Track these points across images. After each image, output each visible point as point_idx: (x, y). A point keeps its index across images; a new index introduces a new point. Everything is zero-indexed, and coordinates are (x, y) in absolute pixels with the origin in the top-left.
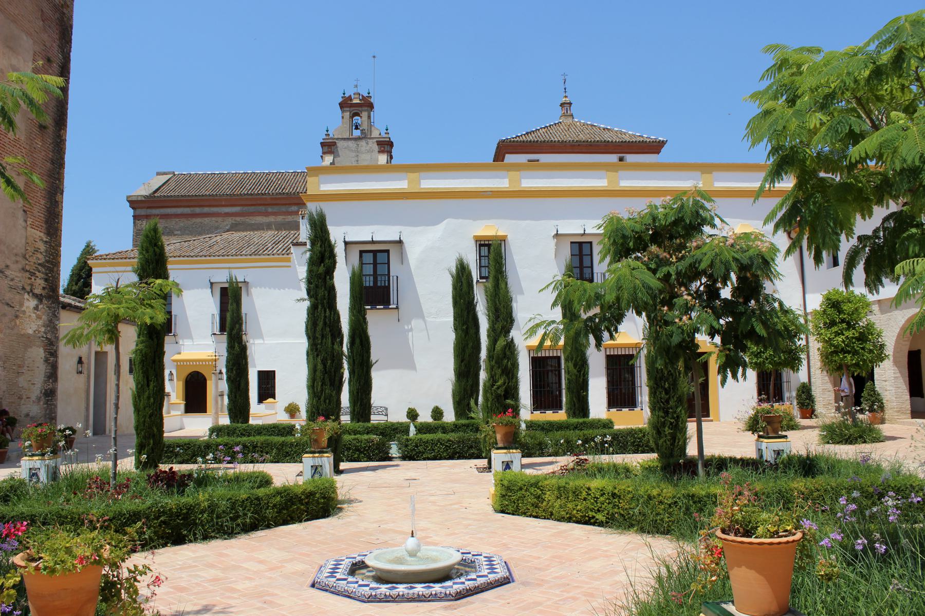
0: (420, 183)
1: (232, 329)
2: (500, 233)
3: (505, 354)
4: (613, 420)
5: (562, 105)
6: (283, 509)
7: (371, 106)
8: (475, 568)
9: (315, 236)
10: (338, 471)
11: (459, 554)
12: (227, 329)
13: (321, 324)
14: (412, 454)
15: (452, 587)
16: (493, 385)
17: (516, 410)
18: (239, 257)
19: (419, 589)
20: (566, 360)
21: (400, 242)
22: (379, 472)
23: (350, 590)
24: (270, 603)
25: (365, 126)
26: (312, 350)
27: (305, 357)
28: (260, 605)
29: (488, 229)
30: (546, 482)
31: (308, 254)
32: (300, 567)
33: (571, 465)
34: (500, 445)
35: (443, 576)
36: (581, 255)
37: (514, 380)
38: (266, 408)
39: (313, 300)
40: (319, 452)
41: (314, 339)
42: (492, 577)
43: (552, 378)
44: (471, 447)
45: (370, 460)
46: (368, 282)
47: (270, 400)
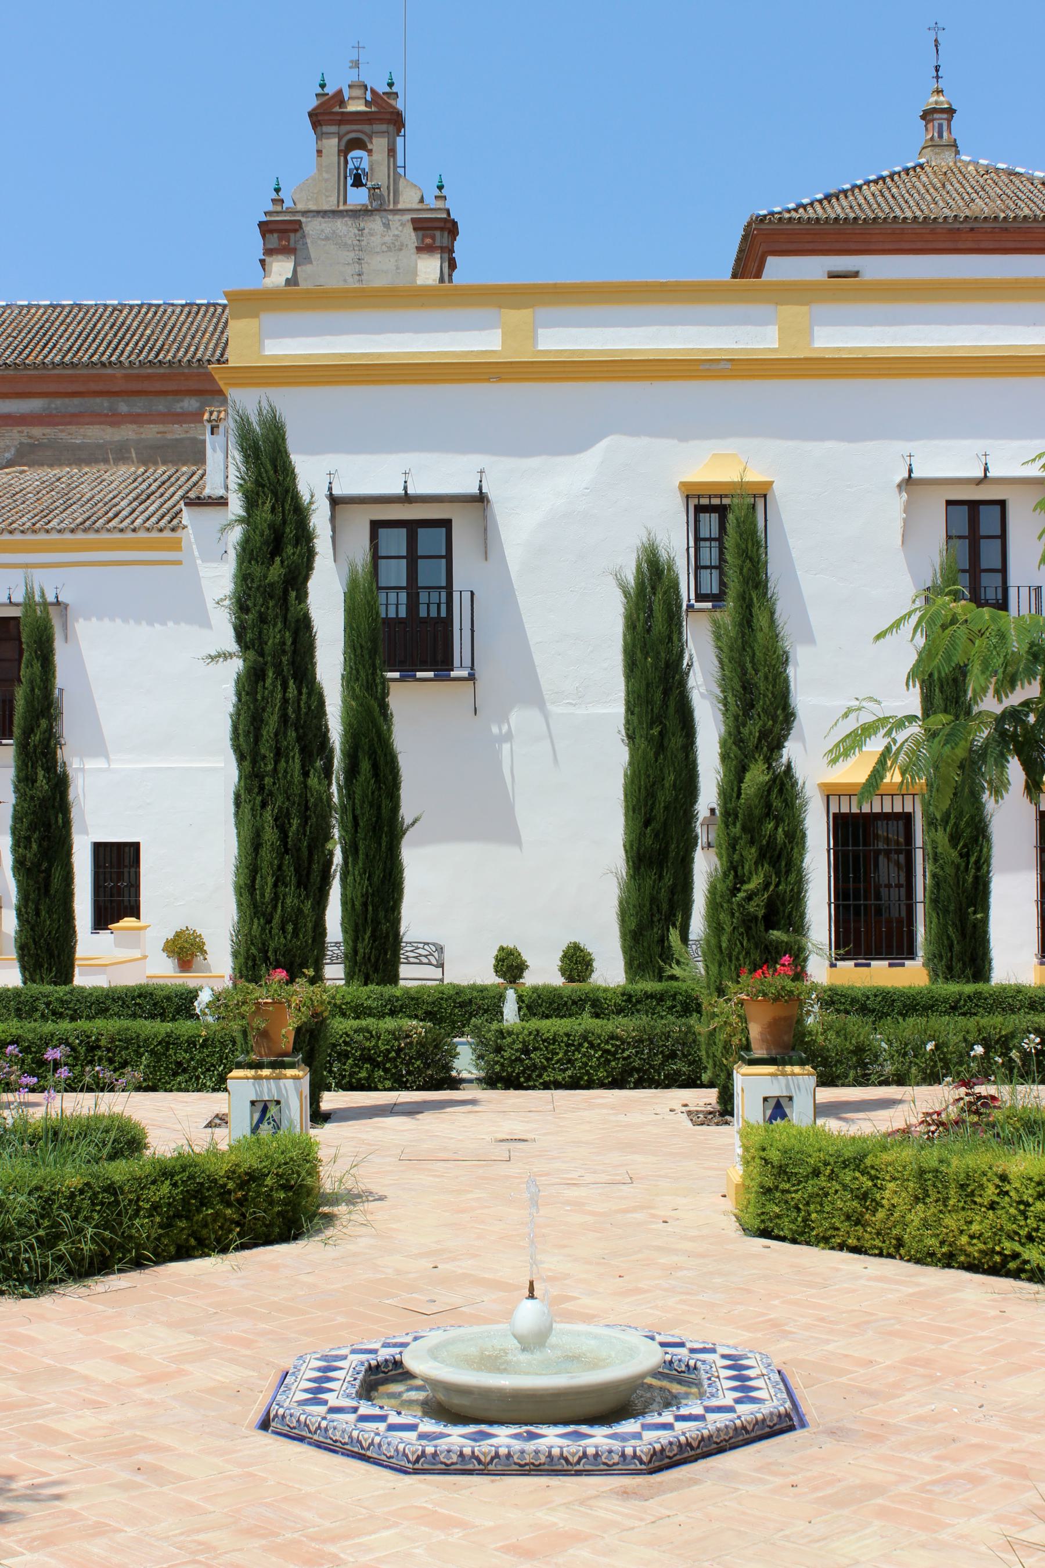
0: (535, 338)
1: (28, 731)
2: (754, 476)
3: (768, 806)
4: (510, 944)
5: (927, 115)
6: (178, 1216)
7: (397, 121)
8: (699, 1385)
9: (258, 483)
10: (319, 1117)
11: (655, 1345)
12: (17, 731)
13: (272, 721)
14: (514, 1070)
15: (638, 1436)
16: (734, 891)
17: (799, 956)
18: (42, 536)
19: (552, 1439)
20: (931, 823)
21: (481, 498)
22: (427, 1118)
23: (366, 1438)
24: (155, 1472)
25: (380, 177)
26: (249, 790)
27: (232, 808)
28: (124, 1476)
29: (718, 464)
30: (886, 1157)
31: (237, 533)
32: (228, 1374)
33: (953, 1112)
34: (758, 1052)
35: (614, 1406)
36: (974, 538)
37: (792, 878)
38: (118, 944)
39: (251, 654)
40: (273, 1065)
41: (254, 762)
42: (746, 1412)
43: (887, 872)
44: (673, 1055)
45: (400, 1085)
46: (394, 606)
47: (128, 922)
